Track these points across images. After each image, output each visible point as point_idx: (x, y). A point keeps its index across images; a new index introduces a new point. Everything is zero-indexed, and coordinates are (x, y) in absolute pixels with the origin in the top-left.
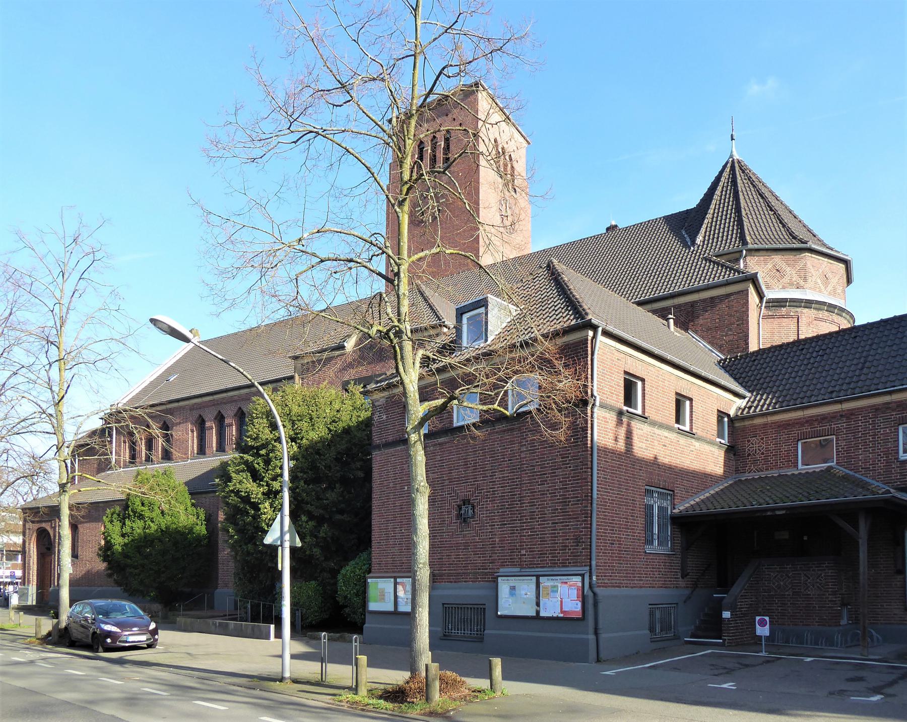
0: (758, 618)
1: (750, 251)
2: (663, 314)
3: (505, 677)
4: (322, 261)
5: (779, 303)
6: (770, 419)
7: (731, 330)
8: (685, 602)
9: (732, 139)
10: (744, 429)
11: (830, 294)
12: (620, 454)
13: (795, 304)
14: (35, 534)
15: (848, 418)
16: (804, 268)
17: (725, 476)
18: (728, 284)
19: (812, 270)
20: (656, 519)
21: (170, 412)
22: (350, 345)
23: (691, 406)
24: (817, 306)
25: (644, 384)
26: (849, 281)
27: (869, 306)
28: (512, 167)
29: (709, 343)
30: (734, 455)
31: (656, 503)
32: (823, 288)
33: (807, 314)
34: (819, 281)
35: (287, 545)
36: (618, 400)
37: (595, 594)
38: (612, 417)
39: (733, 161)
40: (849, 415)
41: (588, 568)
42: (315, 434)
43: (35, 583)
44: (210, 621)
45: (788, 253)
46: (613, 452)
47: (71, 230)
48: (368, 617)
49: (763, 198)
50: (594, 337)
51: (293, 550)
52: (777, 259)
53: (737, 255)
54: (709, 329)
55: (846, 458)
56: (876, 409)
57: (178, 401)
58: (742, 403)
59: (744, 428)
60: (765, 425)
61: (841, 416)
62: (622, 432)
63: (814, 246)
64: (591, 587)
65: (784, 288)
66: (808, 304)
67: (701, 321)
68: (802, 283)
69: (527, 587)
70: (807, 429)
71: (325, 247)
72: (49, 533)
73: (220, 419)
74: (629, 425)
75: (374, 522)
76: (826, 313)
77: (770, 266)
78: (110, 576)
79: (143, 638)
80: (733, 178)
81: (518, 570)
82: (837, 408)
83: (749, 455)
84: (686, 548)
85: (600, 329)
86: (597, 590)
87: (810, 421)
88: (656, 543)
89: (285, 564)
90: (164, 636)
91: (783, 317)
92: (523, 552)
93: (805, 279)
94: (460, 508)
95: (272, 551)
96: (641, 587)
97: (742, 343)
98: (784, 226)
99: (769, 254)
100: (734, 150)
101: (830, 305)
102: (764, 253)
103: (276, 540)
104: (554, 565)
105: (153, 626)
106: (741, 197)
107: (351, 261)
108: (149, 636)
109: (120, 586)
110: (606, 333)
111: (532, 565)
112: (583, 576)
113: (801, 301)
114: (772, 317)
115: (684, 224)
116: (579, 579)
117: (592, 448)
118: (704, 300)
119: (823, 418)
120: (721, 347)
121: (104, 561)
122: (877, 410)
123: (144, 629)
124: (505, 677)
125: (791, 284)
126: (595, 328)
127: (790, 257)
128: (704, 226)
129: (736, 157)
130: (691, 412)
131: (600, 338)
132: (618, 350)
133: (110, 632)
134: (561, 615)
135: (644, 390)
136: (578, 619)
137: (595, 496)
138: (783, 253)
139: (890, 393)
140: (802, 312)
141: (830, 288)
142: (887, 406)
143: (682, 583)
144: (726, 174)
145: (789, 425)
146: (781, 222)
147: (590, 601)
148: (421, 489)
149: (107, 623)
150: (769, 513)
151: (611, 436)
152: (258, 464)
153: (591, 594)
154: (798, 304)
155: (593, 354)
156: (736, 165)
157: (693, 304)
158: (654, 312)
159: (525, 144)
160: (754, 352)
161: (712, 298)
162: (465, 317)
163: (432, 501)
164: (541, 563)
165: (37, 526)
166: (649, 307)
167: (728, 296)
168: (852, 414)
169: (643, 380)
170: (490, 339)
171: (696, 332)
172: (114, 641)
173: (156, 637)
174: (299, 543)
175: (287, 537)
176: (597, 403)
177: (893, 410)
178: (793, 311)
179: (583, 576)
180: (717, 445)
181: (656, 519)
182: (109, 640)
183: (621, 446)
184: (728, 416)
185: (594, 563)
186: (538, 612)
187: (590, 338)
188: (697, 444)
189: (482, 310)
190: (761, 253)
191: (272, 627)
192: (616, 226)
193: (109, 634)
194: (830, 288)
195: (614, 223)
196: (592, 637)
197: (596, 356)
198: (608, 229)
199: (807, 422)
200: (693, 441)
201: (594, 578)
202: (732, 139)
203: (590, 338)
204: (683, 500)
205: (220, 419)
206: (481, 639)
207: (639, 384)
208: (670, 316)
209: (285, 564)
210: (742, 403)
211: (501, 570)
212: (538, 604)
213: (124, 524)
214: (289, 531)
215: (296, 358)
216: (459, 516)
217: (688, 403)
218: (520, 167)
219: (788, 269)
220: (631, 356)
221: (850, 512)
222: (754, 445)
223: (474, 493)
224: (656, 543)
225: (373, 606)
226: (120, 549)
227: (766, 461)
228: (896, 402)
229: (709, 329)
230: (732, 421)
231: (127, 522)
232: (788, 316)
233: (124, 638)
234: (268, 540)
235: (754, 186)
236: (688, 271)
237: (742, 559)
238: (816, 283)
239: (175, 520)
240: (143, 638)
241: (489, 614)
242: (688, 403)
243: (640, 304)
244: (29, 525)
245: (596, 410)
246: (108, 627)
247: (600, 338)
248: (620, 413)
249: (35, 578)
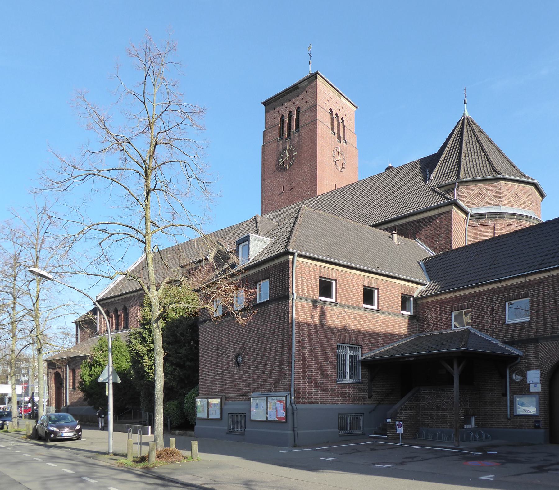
0: (397, 423)
1: (461, 183)
2: (390, 230)
3: (200, 450)
4: (111, 235)
5: (481, 216)
6: (436, 298)
7: (441, 237)
8: (370, 413)
9: (465, 103)
10: (423, 304)
11: (520, 207)
12: (316, 326)
13: (492, 216)
14: (53, 376)
15: (478, 297)
16: (499, 192)
17: (409, 334)
18: (438, 207)
19: (506, 193)
20: (347, 363)
21: (127, 299)
22: (211, 258)
23: (378, 293)
24: (509, 216)
25: (336, 283)
26: (542, 196)
27: (546, 213)
28: (344, 127)
29: (428, 246)
30: (418, 321)
31: (348, 353)
32: (514, 203)
33: (505, 221)
34: (511, 199)
35: (111, 382)
36: (314, 293)
37: (293, 408)
38: (308, 305)
39: (464, 119)
40: (479, 294)
41: (289, 393)
42: (173, 316)
43: (54, 405)
44: (124, 425)
45: (488, 182)
46: (310, 325)
47: (41, 206)
48: (197, 421)
49: (479, 143)
50: (293, 257)
51: (115, 384)
52: (481, 187)
53: (453, 186)
54: (428, 237)
55: (476, 323)
56: (493, 291)
57: (131, 292)
58: (423, 288)
59: (423, 304)
60: (434, 302)
61: (475, 296)
62: (317, 313)
63: (505, 176)
64: (291, 403)
65: (485, 205)
66: (502, 215)
67: (423, 232)
68: (497, 201)
69: (262, 402)
70: (456, 304)
71: (112, 229)
72: (60, 375)
73: (116, 311)
74: (322, 308)
75: (200, 366)
76: (517, 221)
77: (475, 191)
78: (85, 400)
79: (72, 434)
80: (464, 131)
81: (260, 393)
82: (471, 291)
83: (425, 321)
84: (372, 380)
85: (296, 254)
86: (294, 405)
87: (458, 299)
88: (347, 377)
89: (110, 392)
90: (85, 433)
91: (483, 225)
92: (262, 383)
93: (500, 199)
94: (236, 357)
95: (103, 384)
96: (333, 404)
97: (448, 245)
98: (489, 163)
99: (474, 183)
100: (466, 110)
101: (519, 215)
102: (471, 183)
103: (106, 379)
104: (275, 391)
105: (78, 427)
106: (464, 143)
107: (125, 234)
108: (75, 433)
109: (91, 405)
110: (299, 256)
111: (266, 391)
112: (286, 397)
113: (496, 214)
114: (476, 226)
115: (428, 164)
116: (283, 399)
117: (292, 323)
118: (426, 218)
119: (464, 298)
120: (435, 248)
121: (82, 391)
122: (494, 292)
123: (72, 428)
124: (200, 450)
125: (490, 203)
126: (293, 254)
127: (489, 184)
128: (438, 166)
129: (467, 115)
130: (378, 296)
131: (297, 259)
132: (314, 265)
133: (53, 431)
134: (277, 420)
135: (336, 286)
136: (283, 422)
137: (294, 351)
138: (485, 182)
139: (500, 281)
140: (497, 221)
141: (521, 202)
142: (499, 290)
143: (368, 401)
144: (458, 129)
145: (447, 302)
146: (488, 161)
147: (290, 412)
148: (158, 353)
149: (52, 426)
150: (406, 359)
151: (308, 315)
152: (146, 333)
153: (290, 407)
154: (494, 216)
155: (292, 269)
156: (466, 121)
157: (419, 221)
158: (385, 230)
159: (355, 109)
160: (455, 250)
161: (430, 217)
162: (241, 246)
163: (166, 359)
164: (269, 389)
165: (54, 371)
166: (380, 227)
167: (440, 215)
168: (480, 295)
169: (336, 280)
170: (251, 260)
171: (420, 239)
172: (55, 435)
173: (80, 433)
174: (119, 381)
175: (111, 378)
176: (295, 297)
177: (503, 292)
178: (490, 221)
179: (286, 397)
180: (401, 316)
181: (347, 363)
182: (52, 436)
183: (316, 320)
184: (413, 296)
185: (293, 390)
186: (267, 418)
187: (291, 260)
188: (383, 316)
189: (247, 242)
190: (469, 184)
191: (150, 427)
192: (392, 167)
193: (52, 432)
194: (521, 202)
195: (390, 165)
196: (290, 432)
197: (294, 271)
198: (387, 169)
199: (456, 300)
200: (379, 314)
201: (293, 398)
202: (465, 103)
203: (291, 260)
204: (369, 350)
205: (116, 311)
206: (243, 434)
207: (334, 283)
208: (394, 232)
209: (110, 392)
210: (423, 288)
211: (254, 394)
212: (267, 414)
213: (91, 369)
214: (112, 374)
215: (182, 267)
216: (236, 362)
217: (376, 291)
218: (350, 125)
219: (488, 193)
220: (324, 267)
221: (449, 358)
222: (428, 315)
223: (242, 349)
224: (347, 377)
225: (199, 415)
226: (88, 384)
227: (434, 324)
228: (503, 287)
229: (428, 237)
230: (415, 300)
231: (93, 368)
232: (487, 225)
233: (60, 434)
234: (101, 380)
235: (475, 136)
236: (419, 198)
237: (411, 387)
238: (509, 200)
239: (119, 366)
240: (72, 434)
241: (247, 419)
242: (376, 291)
243: (375, 226)
244: (50, 370)
245: (294, 301)
246: (52, 428)
247: (297, 259)
248: (315, 302)
249: (54, 402)
